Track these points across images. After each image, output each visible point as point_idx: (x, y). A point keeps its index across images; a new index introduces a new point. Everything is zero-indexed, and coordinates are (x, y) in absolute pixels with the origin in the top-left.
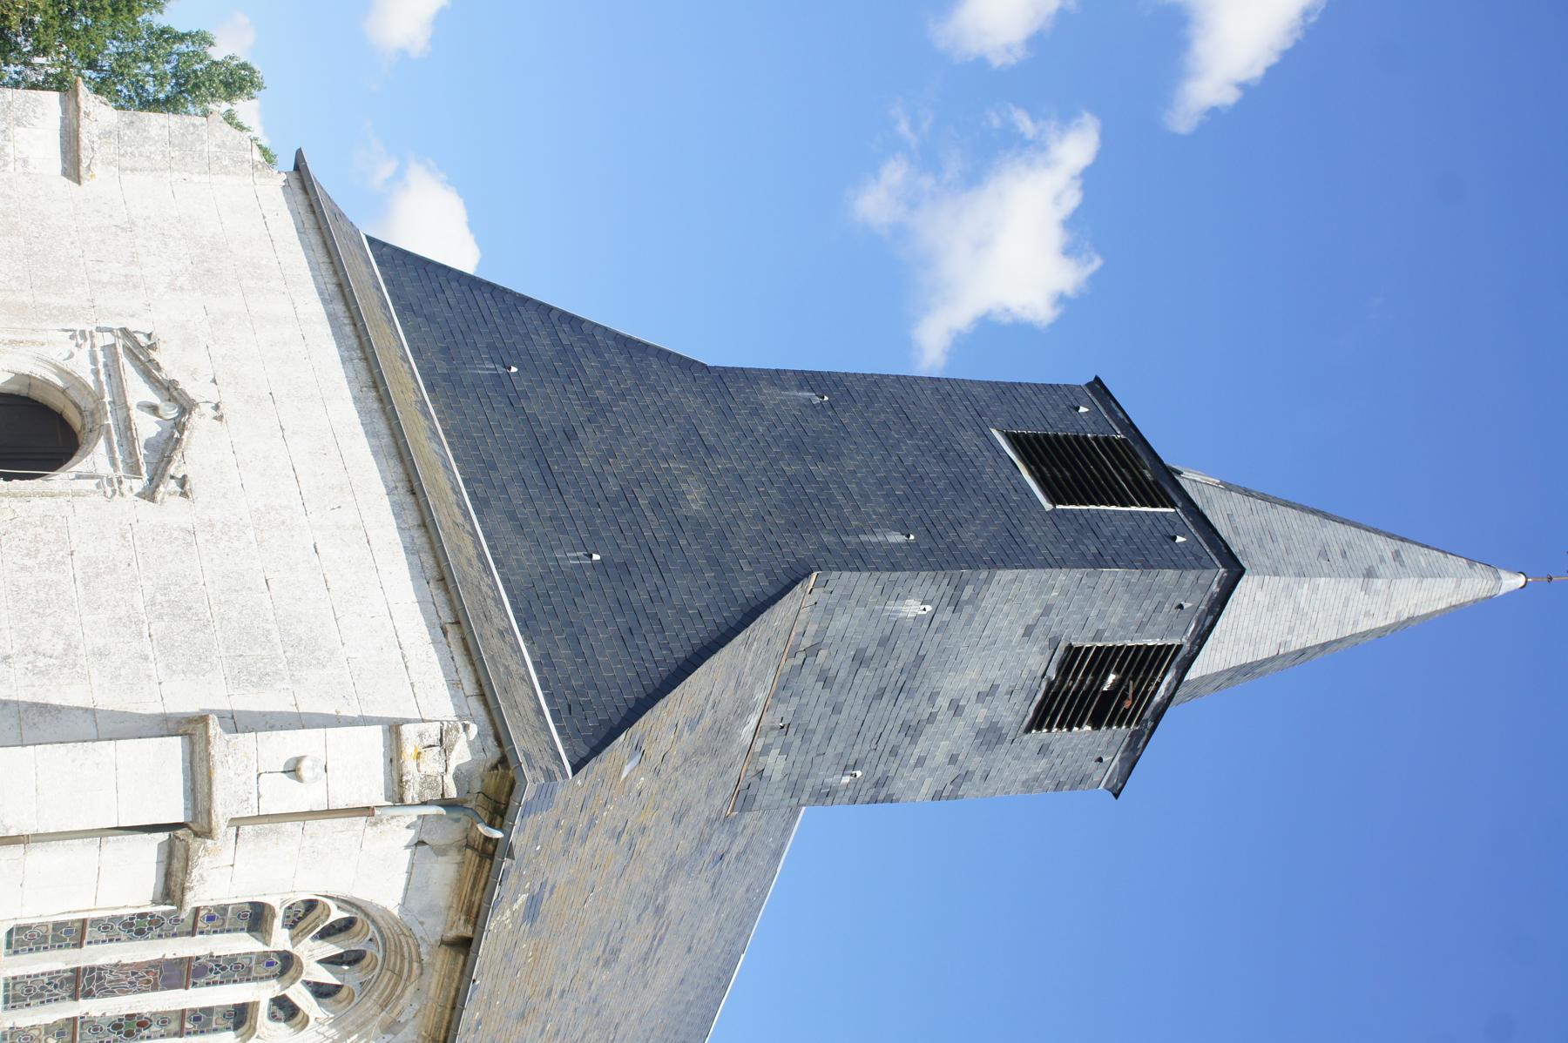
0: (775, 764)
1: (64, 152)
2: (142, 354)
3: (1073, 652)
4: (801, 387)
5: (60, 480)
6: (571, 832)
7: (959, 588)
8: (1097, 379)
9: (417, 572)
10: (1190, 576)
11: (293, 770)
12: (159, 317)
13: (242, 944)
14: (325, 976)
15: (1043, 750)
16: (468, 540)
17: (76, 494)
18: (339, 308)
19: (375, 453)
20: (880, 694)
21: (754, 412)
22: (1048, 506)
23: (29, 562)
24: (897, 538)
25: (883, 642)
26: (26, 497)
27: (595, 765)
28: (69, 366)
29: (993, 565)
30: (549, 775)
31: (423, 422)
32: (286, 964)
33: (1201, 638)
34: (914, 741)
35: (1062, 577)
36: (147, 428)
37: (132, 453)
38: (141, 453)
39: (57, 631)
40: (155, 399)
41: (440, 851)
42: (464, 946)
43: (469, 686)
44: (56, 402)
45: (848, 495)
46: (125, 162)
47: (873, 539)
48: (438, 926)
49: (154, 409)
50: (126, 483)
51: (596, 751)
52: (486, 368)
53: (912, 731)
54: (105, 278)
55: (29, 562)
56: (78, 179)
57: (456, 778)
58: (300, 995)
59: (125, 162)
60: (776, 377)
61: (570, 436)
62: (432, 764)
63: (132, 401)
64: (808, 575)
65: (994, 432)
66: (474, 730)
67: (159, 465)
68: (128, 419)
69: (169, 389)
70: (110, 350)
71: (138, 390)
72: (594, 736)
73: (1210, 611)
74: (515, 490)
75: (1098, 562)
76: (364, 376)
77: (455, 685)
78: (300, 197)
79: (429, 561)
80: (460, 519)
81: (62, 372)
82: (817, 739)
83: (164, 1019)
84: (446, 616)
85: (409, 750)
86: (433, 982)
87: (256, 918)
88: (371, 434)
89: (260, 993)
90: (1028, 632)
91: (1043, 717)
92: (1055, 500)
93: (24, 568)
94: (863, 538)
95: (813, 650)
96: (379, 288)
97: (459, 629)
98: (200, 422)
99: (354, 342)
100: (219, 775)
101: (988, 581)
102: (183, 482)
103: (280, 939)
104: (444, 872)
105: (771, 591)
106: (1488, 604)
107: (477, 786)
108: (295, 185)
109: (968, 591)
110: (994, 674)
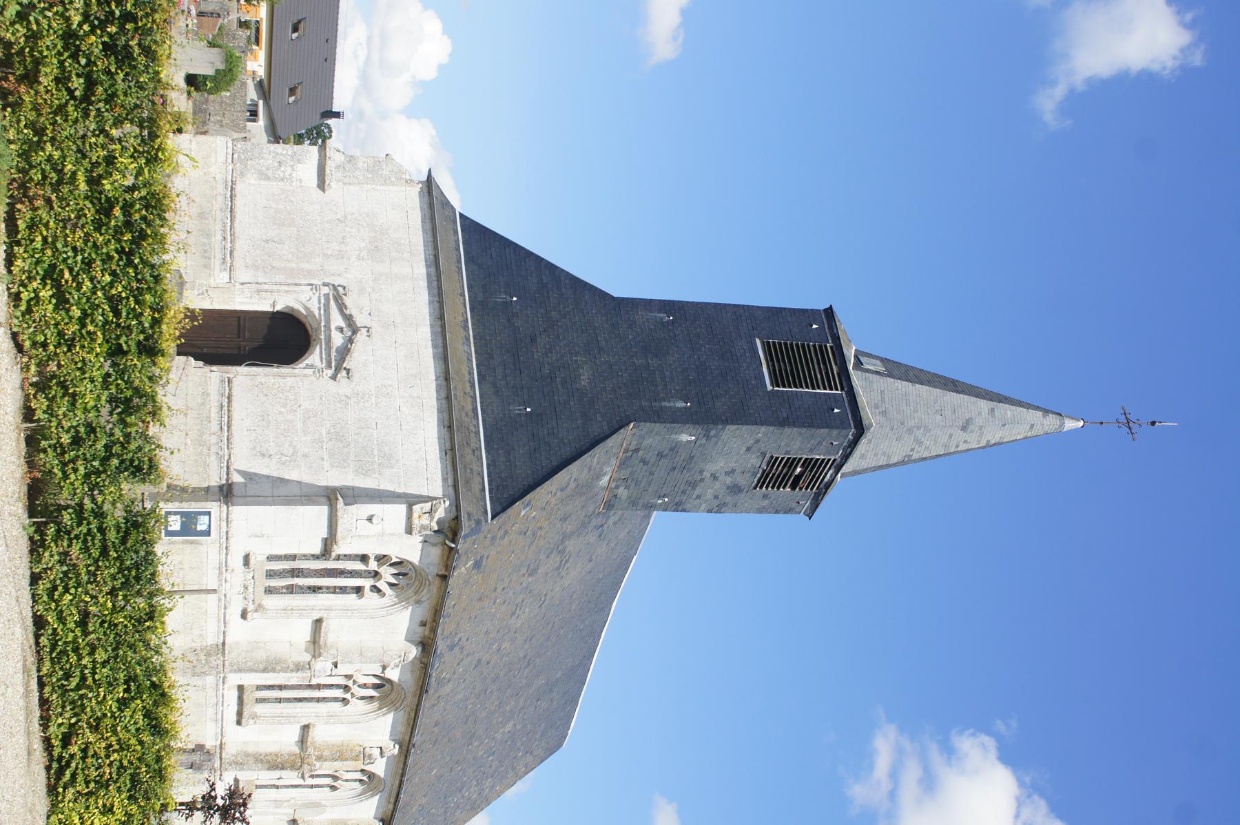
0: (622, 492)
1: (319, 176)
2: (338, 296)
3: (773, 461)
4: (660, 311)
5: (299, 369)
6: (493, 538)
7: (708, 431)
8: (829, 312)
9: (441, 422)
10: (835, 432)
11: (370, 519)
12: (349, 275)
13: (359, 566)
14: (394, 581)
15: (765, 496)
16: (469, 400)
17: (305, 376)
18: (433, 270)
19: (434, 357)
20: (674, 469)
21: (630, 327)
22: (769, 388)
23: (283, 410)
24: (681, 404)
25: (672, 449)
26: (283, 376)
27: (504, 516)
28: (309, 305)
29: (727, 422)
30: (478, 522)
31: (463, 333)
32: (376, 574)
33: (846, 457)
34: (694, 488)
35: (763, 429)
36: (338, 340)
37: (329, 355)
38: (333, 354)
39: (290, 445)
40: (343, 324)
41: (434, 545)
42: (444, 578)
43: (450, 482)
44: (303, 320)
45: (663, 379)
46: (346, 180)
47: (668, 405)
48: (434, 569)
49: (341, 330)
50: (326, 371)
51: (504, 510)
52: (501, 298)
53: (693, 485)
54: (330, 252)
55: (283, 410)
56: (323, 190)
57: (438, 523)
58: (382, 585)
59: (346, 180)
60: (648, 304)
61: (533, 340)
62: (425, 520)
63: (333, 327)
64: (628, 424)
65: (758, 341)
66: (448, 503)
67: (339, 363)
68: (330, 337)
69: (349, 319)
70: (327, 296)
71: (337, 320)
72: (505, 500)
73: (849, 446)
74: (500, 370)
75: (783, 423)
76: (437, 313)
77: (445, 480)
78: (426, 198)
79: (446, 418)
80: (468, 389)
81: (306, 308)
82: (643, 485)
83: (328, 588)
84: (448, 446)
85: (415, 515)
86: (435, 589)
87: (364, 558)
88: (434, 346)
89: (367, 583)
90: (748, 449)
91: (761, 483)
92: (775, 383)
93: (281, 413)
94: (664, 404)
95: (636, 450)
96: (458, 249)
97: (452, 452)
98: (361, 337)
99: (436, 291)
100: (340, 522)
101: (723, 429)
102: (348, 371)
103: (373, 565)
104: (436, 553)
105: (608, 432)
106: (1059, 434)
107: (447, 525)
108: (425, 190)
109: (713, 433)
110: (733, 465)
